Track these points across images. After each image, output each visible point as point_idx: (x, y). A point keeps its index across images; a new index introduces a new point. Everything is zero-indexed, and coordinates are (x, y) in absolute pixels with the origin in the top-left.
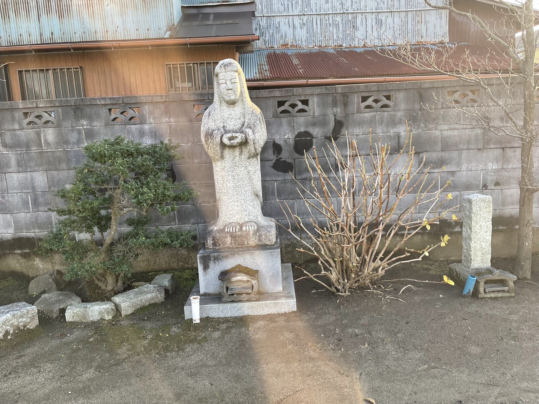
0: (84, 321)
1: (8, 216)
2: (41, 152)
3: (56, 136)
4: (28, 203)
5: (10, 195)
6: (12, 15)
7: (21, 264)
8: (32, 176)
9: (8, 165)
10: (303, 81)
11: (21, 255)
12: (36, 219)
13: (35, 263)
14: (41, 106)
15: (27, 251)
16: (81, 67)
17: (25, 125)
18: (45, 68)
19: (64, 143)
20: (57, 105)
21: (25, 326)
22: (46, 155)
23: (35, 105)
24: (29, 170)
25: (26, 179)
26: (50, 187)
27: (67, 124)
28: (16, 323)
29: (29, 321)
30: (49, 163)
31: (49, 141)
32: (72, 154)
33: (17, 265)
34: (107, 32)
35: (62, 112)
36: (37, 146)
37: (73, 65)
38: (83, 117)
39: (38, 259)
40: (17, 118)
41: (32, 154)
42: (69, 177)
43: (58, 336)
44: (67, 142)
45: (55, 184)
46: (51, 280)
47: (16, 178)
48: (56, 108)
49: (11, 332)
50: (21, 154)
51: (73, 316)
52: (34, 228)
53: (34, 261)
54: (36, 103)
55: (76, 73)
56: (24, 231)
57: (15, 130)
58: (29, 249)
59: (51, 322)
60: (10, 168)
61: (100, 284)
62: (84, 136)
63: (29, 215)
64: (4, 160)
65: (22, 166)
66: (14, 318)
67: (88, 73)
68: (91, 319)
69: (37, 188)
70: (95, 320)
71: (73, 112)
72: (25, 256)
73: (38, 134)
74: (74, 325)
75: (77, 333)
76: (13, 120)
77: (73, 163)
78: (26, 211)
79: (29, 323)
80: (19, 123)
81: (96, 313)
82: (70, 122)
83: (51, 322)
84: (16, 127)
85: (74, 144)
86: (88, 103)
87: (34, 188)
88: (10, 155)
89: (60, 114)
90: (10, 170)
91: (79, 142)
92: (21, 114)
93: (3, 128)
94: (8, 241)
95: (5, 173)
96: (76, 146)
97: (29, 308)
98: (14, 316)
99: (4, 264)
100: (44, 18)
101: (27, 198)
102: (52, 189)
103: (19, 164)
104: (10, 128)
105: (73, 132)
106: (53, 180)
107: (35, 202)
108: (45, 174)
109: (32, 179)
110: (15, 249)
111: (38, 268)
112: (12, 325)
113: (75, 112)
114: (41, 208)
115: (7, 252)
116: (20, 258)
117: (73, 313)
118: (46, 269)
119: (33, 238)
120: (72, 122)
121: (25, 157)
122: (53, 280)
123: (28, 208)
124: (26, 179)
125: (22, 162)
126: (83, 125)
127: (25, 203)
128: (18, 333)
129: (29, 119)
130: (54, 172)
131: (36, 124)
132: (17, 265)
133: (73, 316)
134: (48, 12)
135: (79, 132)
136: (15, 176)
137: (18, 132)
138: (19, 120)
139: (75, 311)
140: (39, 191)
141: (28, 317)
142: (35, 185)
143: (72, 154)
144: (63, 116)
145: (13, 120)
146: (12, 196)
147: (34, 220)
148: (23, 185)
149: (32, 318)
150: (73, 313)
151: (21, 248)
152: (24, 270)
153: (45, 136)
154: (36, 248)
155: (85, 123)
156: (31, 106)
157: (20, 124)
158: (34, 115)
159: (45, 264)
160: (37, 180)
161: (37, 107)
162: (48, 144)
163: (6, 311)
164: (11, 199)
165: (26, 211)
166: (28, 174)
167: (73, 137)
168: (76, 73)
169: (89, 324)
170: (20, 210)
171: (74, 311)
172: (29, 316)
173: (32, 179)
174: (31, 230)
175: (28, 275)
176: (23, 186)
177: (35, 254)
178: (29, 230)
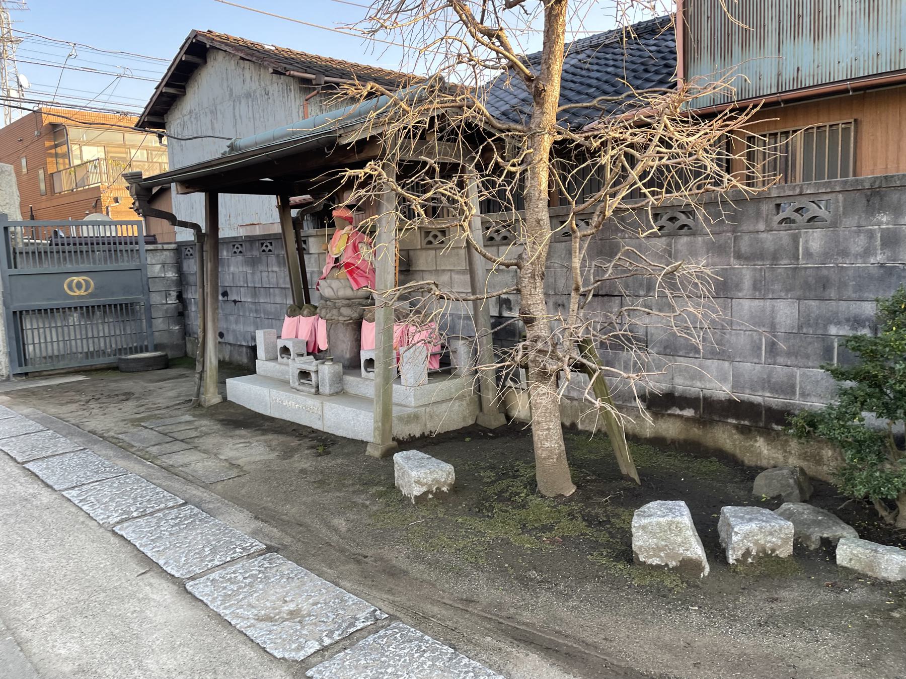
0: (870, 573)
1: (726, 364)
2: (796, 268)
3: (826, 242)
4: (760, 348)
5: (733, 332)
6: (737, 49)
7: (735, 440)
8: (774, 306)
9: (738, 287)
10: (18, 104)
11: (736, 427)
12: (770, 376)
13: (757, 444)
14: (808, 192)
15: (747, 423)
16: (855, 120)
17: (775, 225)
18: (791, 129)
19: (838, 254)
20: (838, 189)
21: (773, 551)
22: (803, 272)
23: (797, 191)
24: (770, 296)
25: (763, 310)
26: (800, 327)
27: (851, 222)
28: (762, 542)
29: (780, 543)
30: (807, 286)
31: (812, 251)
32: (851, 273)
33: (728, 441)
34: (900, 51)
35: (845, 200)
36: (790, 259)
37: (840, 120)
38: (881, 209)
39: (762, 439)
40: (765, 213)
41: (779, 270)
42: (837, 313)
43: (827, 585)
44: (845, 253)
45: (812, 322)
46: (791, 481)
47: (746, 307)
48: (834, 194)
49: (754, 553)
50: (761, 269)
51: (851, 560)
52: (763, 389)
53: (756, 441)
54: (801, 188)
55: (846, 131)
56: (747, 391)
57: (757, 232)
58: (750, 421)
59: (814, 557)
60: (740, 290)
61: (882, 513)
62: (878, 242)
63: (758, 367)
64: (734, 278)
65: (760, 289)
66: (761, 532)
67: (866, 128)
68: (884, 575)
69: (778, 326)
70: (892, 579)
71: (864, 201)
72: (743, 431)
73: (795, 239)
74: (852, 576)
75: (859, 594)
76: (758, 215)
77: (850, 288)
78: (756, 360)
79: (780, 547)
80: (766, 221)
81: (896, 568)
82: (856, 217)
83: (814, 557)
84: (761, 226)
85: (856, 256)
86: (898, 183)
87: (773, 327)
88: (744, 271)
89: (841, 204)
90: (740, 295)
91: (868, 252)
92: (772, 206)
93: (740, 229)
94: (720, 402)
95: (732, 299)
96: (860, 261)
97: (782, 522)
98: (761, 528)
99: (709, 435)
100: (787, 46)
101: (761, 340)
102: (805, 330)
103: (755, 287)
104: (751, 228)
105: (858, 236)
106: (808, 315)
107: (772, 348)
108: (796, 305)
109: (773, 311)
110: (728, 417)
111: (760, 453)
112: (756, 543)
113: (868, 201)
114: (780, 360)
115: (716, 418)
116: (734, 432)
117: (851, 553)
118: (773, 458)
119: (759, 405)
120: (859, 218)
121: (767, 274)
122: (795, 481)
123: (759, 356)
124: (763, 310)
125: (761, 282)
126: (879, 223)
127: (757, 348)
128: (761, 558)
129: (782, 215)
130: (812, 303)
131: (794, 221)
132: (728, 441)
133: (851, 560)
134: (797, 32)
135: (871, 235)
136: (746, 303)
137: (763, 236)
138: (767, 215)
139: (855, 552)
140: (781, 329)
141: (780, 538)
142: (777, 320)
143: (851, 273)
144: (844, 208)
145: (758, 215)
146: (736, 334)
147: (765, 377)
148: (757, 320)
149: (785, 541)
150: (851, 553)
151: (737, 417)
152: (738, 452)
153: (807, 242)
154: (761, 420)
155: (884, 219)
156: (791, 193)
157: (767, 222)
158: (794, 206)
159: (773, 451)
160: (781, 312)
161: (801, 194)
162: (808, 254)
163: (747, 516)
164: (733, 339)
165: (756, 360)
166: (768, 302)
167: (858, 244)
168: (846, 131)
169: (881, 584)
170: (745, 357)
171: (851, 550)
172: (782, 536)
173: (773, 311)
174: (758, 391)
175: (743, 462)
176: (757, 320)
177: (759, 432)
178: (754, 391)
